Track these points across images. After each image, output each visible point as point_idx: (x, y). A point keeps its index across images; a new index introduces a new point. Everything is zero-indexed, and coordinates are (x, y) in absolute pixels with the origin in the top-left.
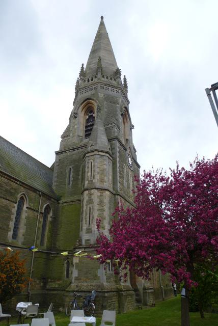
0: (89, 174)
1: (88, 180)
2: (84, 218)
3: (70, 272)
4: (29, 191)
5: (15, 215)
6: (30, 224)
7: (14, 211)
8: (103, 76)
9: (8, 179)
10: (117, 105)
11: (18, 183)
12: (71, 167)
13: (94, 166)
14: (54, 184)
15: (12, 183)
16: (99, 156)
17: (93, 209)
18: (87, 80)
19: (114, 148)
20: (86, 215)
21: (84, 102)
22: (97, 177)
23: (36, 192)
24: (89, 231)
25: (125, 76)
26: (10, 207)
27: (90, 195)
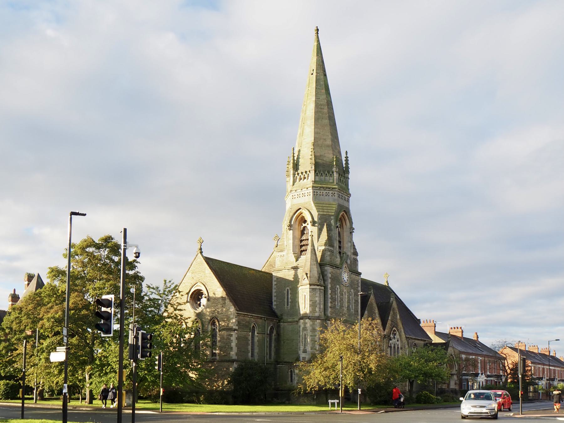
2: (301, 342)
3: (293, 378)
4: (257, 319)
5: (251, 341)
7: (250, 338)
9: (243, 316)
11: (250, 316)
14: (274, 303)
17: (307, 335)
20: (302, 339)
24: (305, 351)
25: (347, 152)
26: (247, 336)
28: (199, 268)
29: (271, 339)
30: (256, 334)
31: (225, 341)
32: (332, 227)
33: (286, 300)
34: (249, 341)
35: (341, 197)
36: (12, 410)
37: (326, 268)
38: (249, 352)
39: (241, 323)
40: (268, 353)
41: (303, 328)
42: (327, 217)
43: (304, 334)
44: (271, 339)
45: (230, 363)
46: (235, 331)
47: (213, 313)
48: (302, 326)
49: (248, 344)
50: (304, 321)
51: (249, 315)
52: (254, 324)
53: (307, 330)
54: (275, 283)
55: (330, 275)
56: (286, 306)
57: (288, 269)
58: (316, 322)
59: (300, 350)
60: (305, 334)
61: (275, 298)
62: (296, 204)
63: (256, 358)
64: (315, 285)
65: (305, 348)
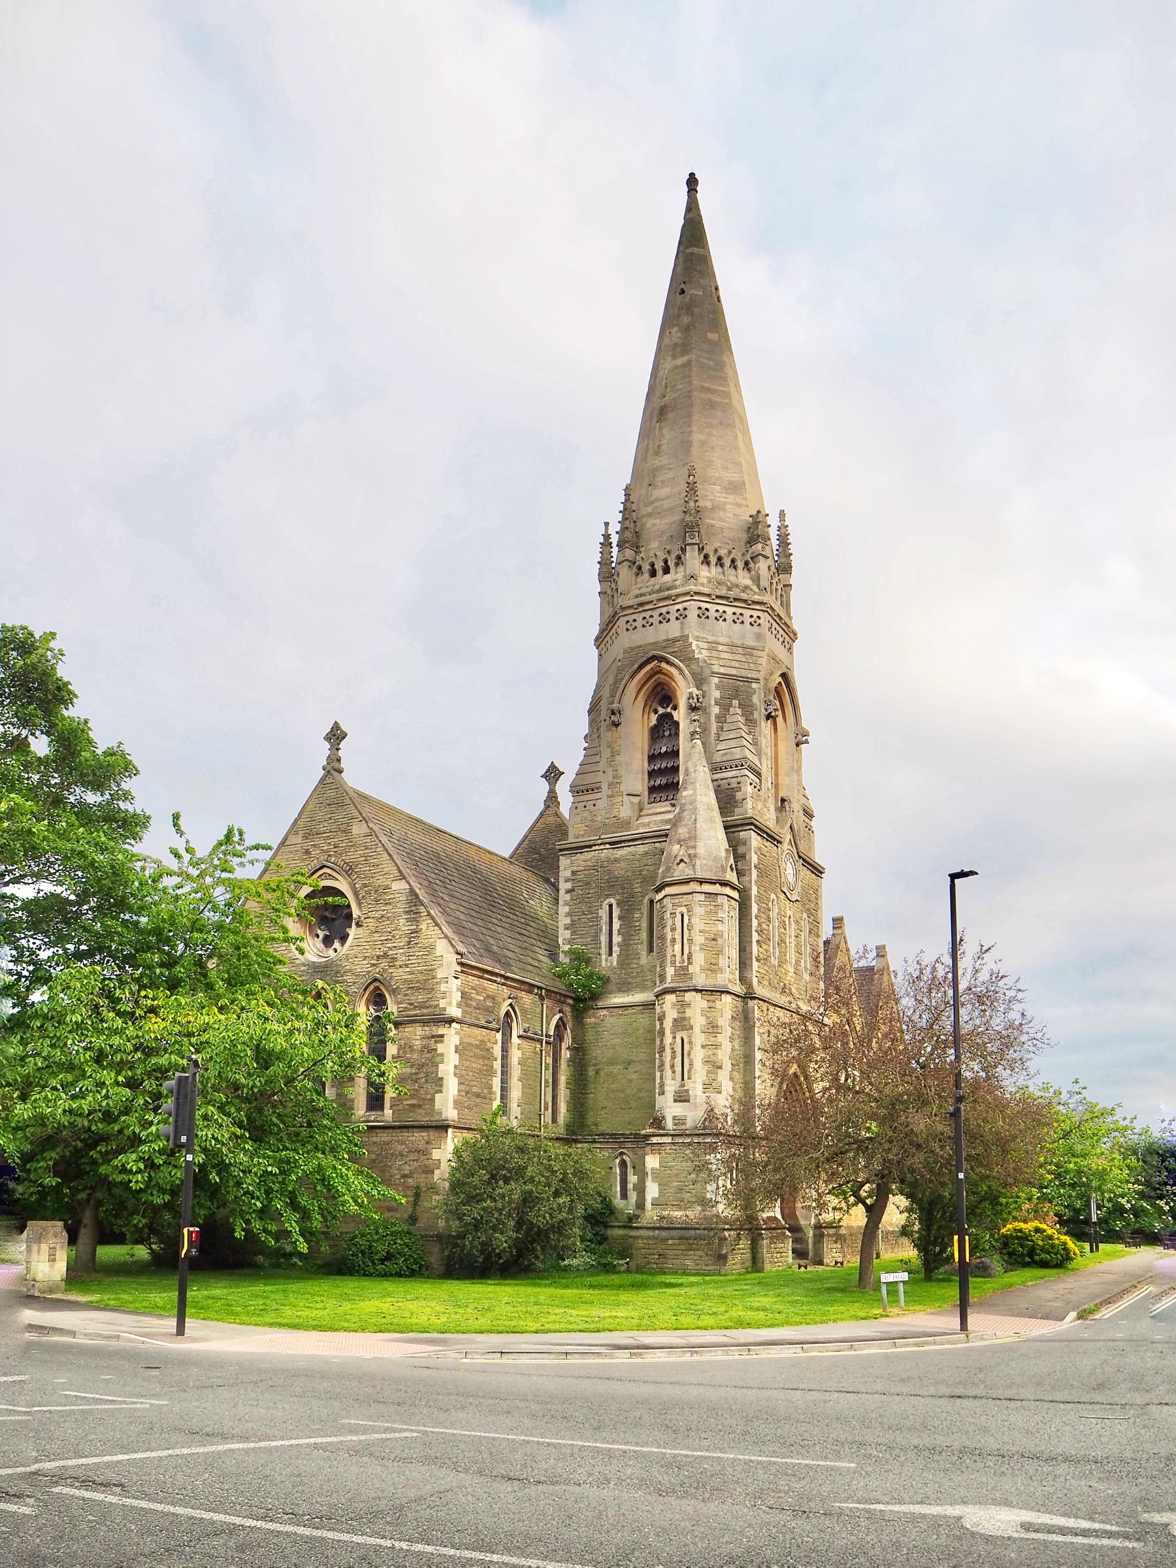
0: (678, 947)
1: (673, 963)
6: (530, 1077)
7: (497, 1050)
8: (706, 556)
10: (754, 686)
11: (498, 979)
12: (613, 901)
13: (690, 941)
15: (486, 984)
16: (702, 897)
17: (690, 1043)
18: (646, 567)
19: (743, 856)
20: (673, 1058)
21: (641, 667)
22: (699, 959)
23: (530, 992)
24: (682, 1097)
25: (782, 514)
26: (489, 1045)
27: (683, 1006)
28: (330, 819)
29: (556, 1060)
30: (515, 1040)
31: (415, 1056)
32: (756, 715)
33: (604, 939)
34: (496, 1059)
35: (775, 632)
36: (724, 1281)
37: (741, 833)
38: (495, 1099)
39: (471, 999)
40: (550, 1104)
41: (675, 1020)
42: (741, 684)
43: (679, 1041)
44: (556, 1060)
45: (432, 1134)
46: (454, 1025)
47: (374, 965)
48: (671, 1014)
49: (491, 1072)
50: (680, 999)
51: (497, 975)
52: (511, 1005)
53: (691, 1027)
54: (569, 886)
55: (754, 859)
56: (603, 957)
57: (610, 843)
58: (718, 1002)
59: (662, 1093)
60: (683, 1040)
61: (568, 932)
62: (637, 647)
63: (514, 1119)
64: (715, 883)
65: (683, 1086)
